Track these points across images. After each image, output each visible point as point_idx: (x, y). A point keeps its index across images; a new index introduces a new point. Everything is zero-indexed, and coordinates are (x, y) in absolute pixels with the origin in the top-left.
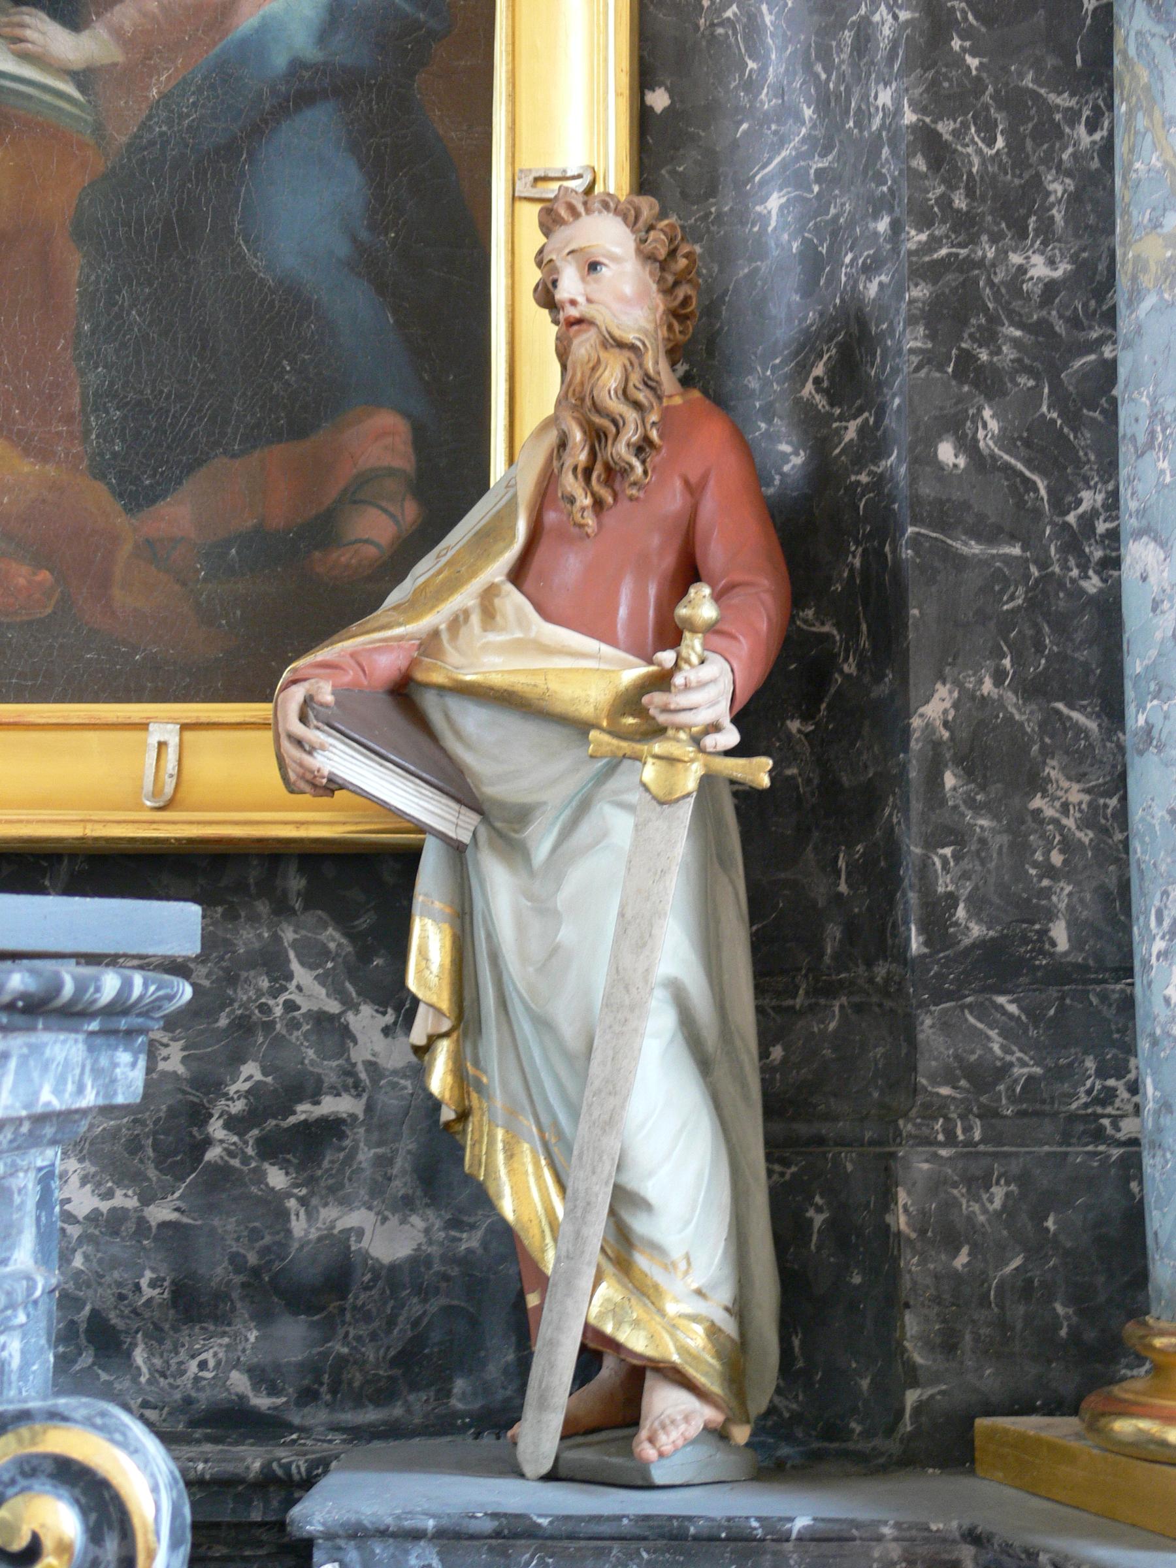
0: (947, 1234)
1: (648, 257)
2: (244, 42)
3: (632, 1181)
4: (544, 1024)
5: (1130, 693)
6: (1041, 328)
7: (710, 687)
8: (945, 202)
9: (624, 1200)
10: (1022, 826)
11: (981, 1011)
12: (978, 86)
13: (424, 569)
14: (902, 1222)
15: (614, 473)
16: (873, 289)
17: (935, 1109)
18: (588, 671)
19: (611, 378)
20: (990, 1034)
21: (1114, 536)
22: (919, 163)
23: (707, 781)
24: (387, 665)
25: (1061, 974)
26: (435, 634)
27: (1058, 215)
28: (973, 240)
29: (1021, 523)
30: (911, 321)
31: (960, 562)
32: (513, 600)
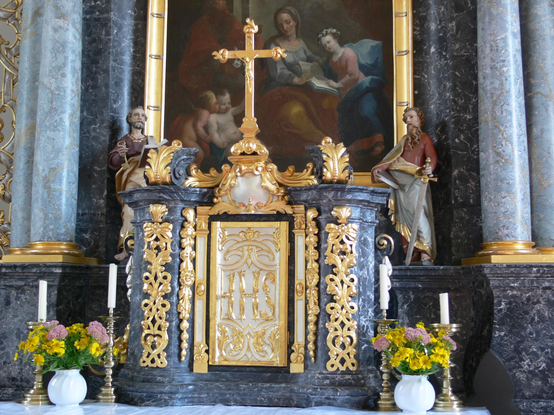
0: (457, 237)
1: (418, 116)
2: (359, 84)
3: (420, 229)
4: (407, 211)
5: (480, 170)
6: (469, 124)
7: (429, 169)
8: (456, 108)
9: (419, 232)
10: (466, 187)
11: (462, 210)
12: (460, 93)
13: (388, 155)
14: (452, 236)
15: (415, 143)
16: (446, 119)
17: (456, 222)
18: (413, 168)
19: (414, 131)
20: (463, 213)
21: (478, 151)
22: (453, 103)
23: (430, 181)
24: (385, 167)
25: (471, 206)
26: (391, 163)
27: (471, 110)
28: (460, 113)
29: (466, 149)
30: (452, 123)
31: (458, 154)
32: (402, 159)
